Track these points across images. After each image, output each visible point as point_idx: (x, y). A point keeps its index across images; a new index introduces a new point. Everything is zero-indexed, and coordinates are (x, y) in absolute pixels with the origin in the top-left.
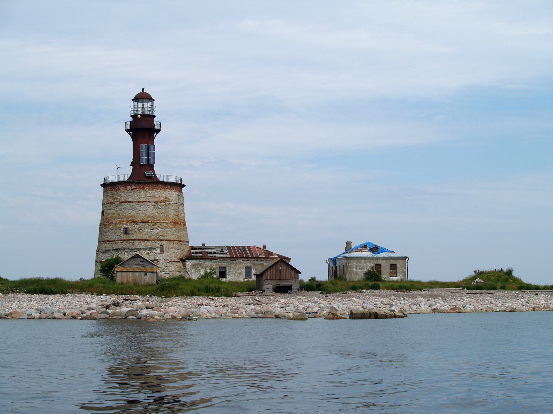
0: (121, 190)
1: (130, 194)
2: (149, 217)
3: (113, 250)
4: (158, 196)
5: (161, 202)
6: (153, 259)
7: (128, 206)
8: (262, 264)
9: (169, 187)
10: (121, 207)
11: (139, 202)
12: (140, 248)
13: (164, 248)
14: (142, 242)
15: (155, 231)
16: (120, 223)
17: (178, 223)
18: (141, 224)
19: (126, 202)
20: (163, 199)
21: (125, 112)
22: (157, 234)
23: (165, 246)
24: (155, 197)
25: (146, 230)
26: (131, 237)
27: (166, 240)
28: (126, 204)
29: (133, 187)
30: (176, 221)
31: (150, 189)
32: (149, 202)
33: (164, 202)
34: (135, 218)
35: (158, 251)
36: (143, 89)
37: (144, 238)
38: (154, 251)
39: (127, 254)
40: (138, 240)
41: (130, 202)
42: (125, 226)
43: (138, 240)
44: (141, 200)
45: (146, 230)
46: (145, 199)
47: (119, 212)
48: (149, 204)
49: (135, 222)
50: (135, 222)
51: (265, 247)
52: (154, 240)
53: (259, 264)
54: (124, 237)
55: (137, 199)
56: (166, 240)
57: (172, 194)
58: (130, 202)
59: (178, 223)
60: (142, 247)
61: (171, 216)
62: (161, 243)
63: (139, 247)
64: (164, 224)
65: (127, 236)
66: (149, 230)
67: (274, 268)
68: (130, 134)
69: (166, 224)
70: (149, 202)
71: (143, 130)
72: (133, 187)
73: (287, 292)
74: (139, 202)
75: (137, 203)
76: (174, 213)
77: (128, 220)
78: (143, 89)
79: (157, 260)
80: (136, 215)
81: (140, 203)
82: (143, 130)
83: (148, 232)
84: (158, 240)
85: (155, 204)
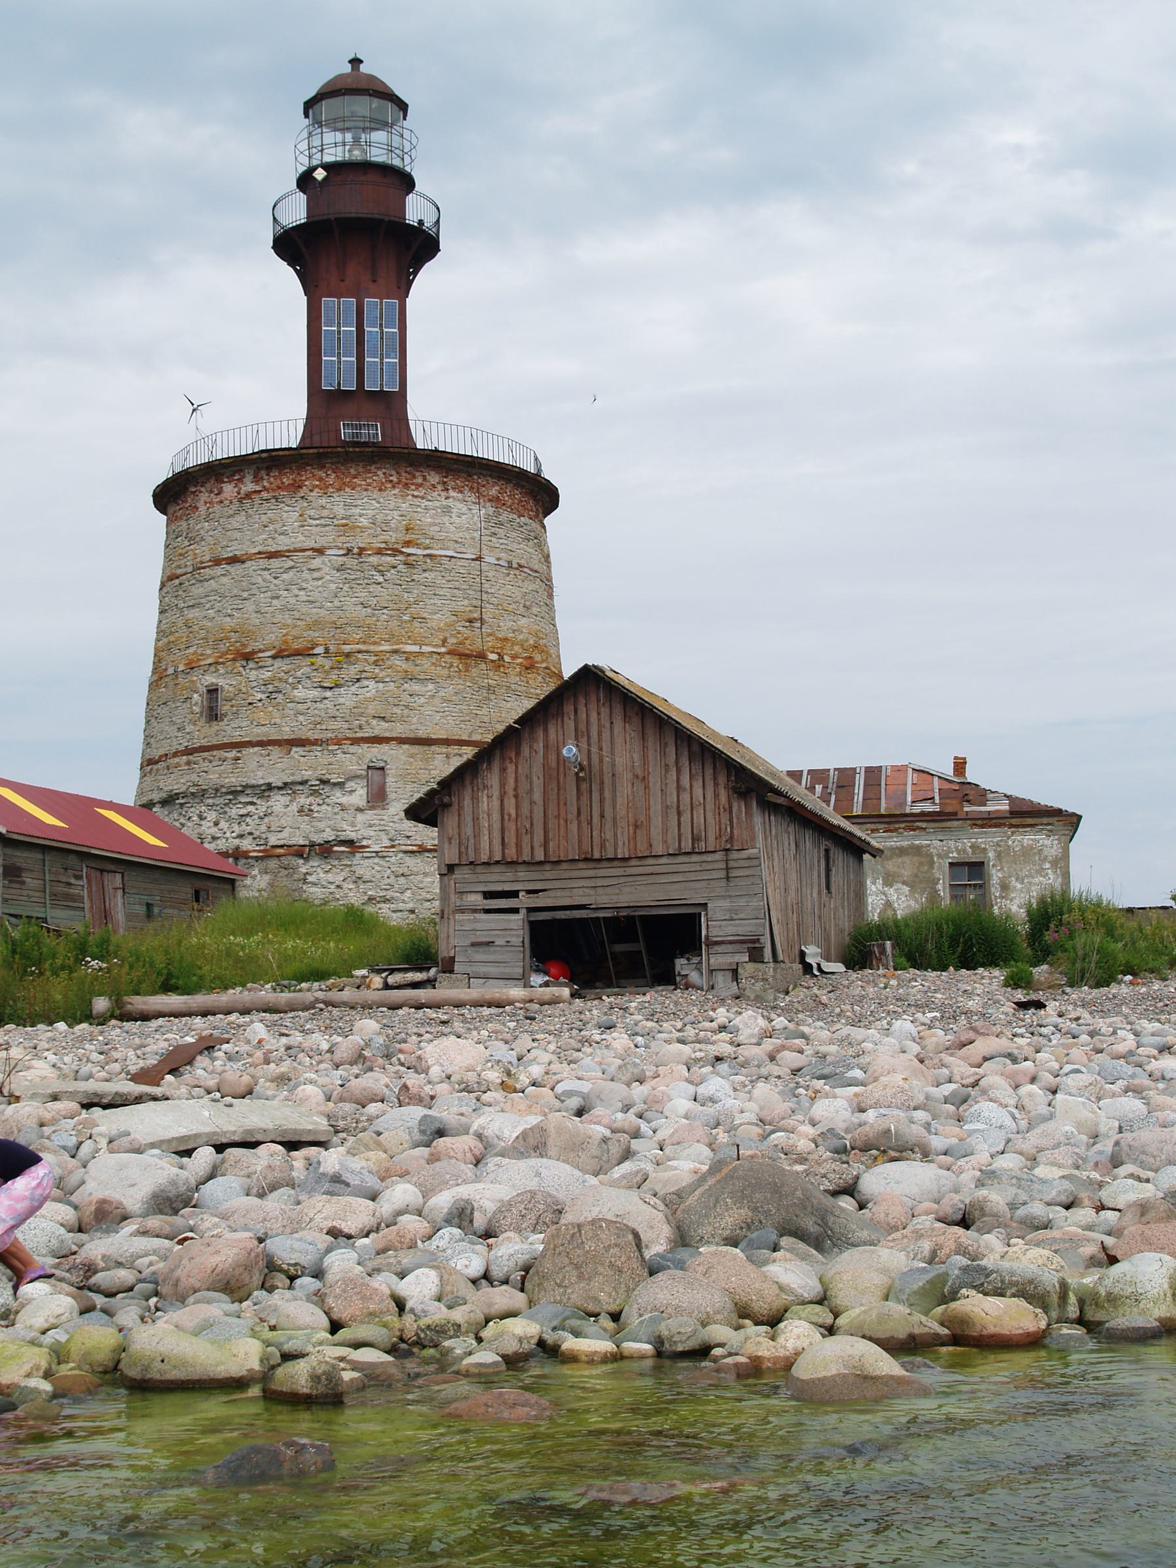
0: (202, 509)
1: (234, 523)
2: (316, 624)
3: (165, 802)
4: (364, 522)
5: (379, 552)
6: (329, 835)
7: (225, 579)
8: (917, 850)
9: (434, 478)
10: (197, 590)
11: (271, 555)
12: (270, 787)
13: (390, 780)
14: (276, 751)
15: (347, 697)
16: (191, 667)
17: (482, 656)
18: (278, 663)
19: (217, 562)
20: (392, 537)
21: (270, 167)
22: (357, 711)
23: (391, 770)
24: (347, 527)
25: (300, 693)
26: (231, 730)
27: (402, 741)
28: (218, 570)
29: (249, 486)
30: (468, 647)
31: (324, 488)
32: (320, 551)
33: (396, 552)
34: (251, 635)
35: (359, 795)
36: (356, 62)
37: (287, 733)
38: (338, 796)
39: (212, 816)
40: (261, 744)
41: (234, 560)
42: (210, 679)
43: (261, 744)
44: (283, 543)
45: (300, 693)
46: (300, 541)
47: (192, 614)
48: (317, 562)
49: (248, 657)
50: (248, 657)
51: (960, 766)
52: (338, 742)
53: (902, 851)
54: (205, 733)
55: (261, 541)
56: (402, 741)
57: (447, 510)
58: (234, 560)
59: (482, 656)
60: (276, 781)
61: (440, 619)
62: (374, 753)
63: (259, 778)
64: (398, 662)
65: (215, 726)
66: (315, 693)
67: (534, 752)
68: (295, 270)
69: (408, 657)
70: (320, 551)
71: (356, 238)
72: (249, 486)
73: (666, 977)
74: (271, 555)
75: (263, 563)
76: (463, 605)
77: (223, 647)
78: (356, 62)
79: (350, 843)
80: (255, 619)
81: (275, 563)
82: (356, 238)
83: (305, 701)
84: (356, 741)
85: (351, 562)
